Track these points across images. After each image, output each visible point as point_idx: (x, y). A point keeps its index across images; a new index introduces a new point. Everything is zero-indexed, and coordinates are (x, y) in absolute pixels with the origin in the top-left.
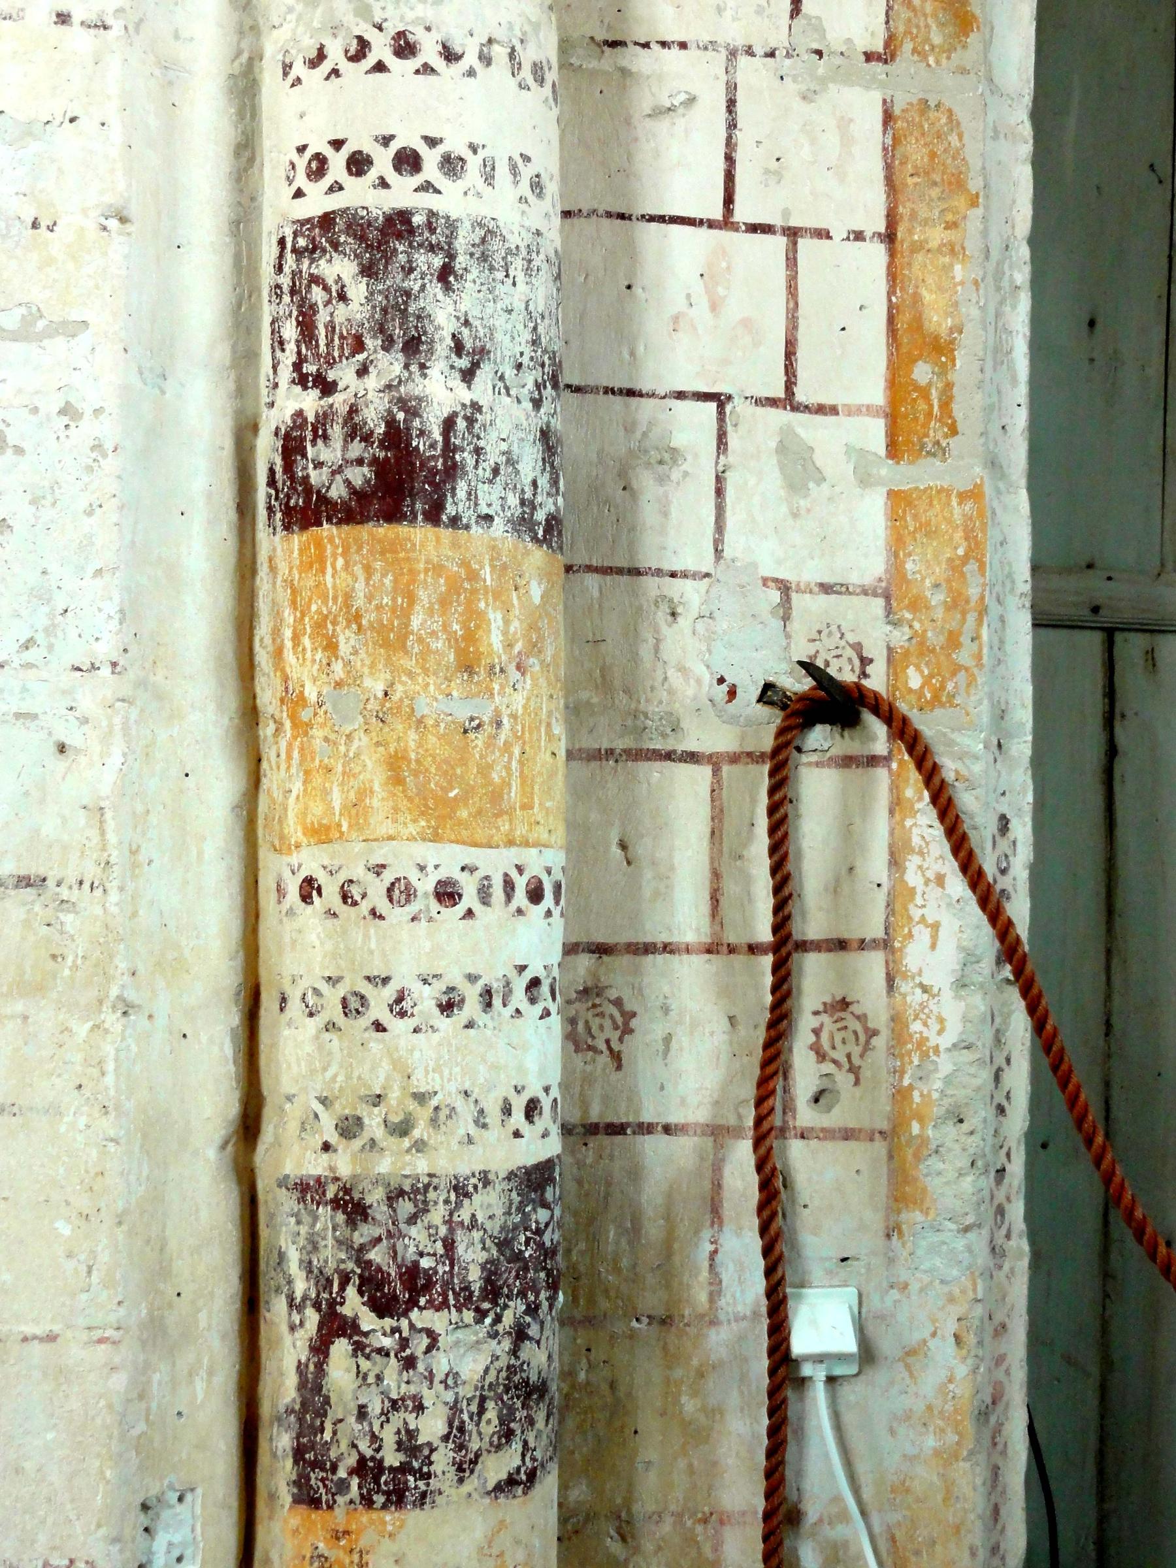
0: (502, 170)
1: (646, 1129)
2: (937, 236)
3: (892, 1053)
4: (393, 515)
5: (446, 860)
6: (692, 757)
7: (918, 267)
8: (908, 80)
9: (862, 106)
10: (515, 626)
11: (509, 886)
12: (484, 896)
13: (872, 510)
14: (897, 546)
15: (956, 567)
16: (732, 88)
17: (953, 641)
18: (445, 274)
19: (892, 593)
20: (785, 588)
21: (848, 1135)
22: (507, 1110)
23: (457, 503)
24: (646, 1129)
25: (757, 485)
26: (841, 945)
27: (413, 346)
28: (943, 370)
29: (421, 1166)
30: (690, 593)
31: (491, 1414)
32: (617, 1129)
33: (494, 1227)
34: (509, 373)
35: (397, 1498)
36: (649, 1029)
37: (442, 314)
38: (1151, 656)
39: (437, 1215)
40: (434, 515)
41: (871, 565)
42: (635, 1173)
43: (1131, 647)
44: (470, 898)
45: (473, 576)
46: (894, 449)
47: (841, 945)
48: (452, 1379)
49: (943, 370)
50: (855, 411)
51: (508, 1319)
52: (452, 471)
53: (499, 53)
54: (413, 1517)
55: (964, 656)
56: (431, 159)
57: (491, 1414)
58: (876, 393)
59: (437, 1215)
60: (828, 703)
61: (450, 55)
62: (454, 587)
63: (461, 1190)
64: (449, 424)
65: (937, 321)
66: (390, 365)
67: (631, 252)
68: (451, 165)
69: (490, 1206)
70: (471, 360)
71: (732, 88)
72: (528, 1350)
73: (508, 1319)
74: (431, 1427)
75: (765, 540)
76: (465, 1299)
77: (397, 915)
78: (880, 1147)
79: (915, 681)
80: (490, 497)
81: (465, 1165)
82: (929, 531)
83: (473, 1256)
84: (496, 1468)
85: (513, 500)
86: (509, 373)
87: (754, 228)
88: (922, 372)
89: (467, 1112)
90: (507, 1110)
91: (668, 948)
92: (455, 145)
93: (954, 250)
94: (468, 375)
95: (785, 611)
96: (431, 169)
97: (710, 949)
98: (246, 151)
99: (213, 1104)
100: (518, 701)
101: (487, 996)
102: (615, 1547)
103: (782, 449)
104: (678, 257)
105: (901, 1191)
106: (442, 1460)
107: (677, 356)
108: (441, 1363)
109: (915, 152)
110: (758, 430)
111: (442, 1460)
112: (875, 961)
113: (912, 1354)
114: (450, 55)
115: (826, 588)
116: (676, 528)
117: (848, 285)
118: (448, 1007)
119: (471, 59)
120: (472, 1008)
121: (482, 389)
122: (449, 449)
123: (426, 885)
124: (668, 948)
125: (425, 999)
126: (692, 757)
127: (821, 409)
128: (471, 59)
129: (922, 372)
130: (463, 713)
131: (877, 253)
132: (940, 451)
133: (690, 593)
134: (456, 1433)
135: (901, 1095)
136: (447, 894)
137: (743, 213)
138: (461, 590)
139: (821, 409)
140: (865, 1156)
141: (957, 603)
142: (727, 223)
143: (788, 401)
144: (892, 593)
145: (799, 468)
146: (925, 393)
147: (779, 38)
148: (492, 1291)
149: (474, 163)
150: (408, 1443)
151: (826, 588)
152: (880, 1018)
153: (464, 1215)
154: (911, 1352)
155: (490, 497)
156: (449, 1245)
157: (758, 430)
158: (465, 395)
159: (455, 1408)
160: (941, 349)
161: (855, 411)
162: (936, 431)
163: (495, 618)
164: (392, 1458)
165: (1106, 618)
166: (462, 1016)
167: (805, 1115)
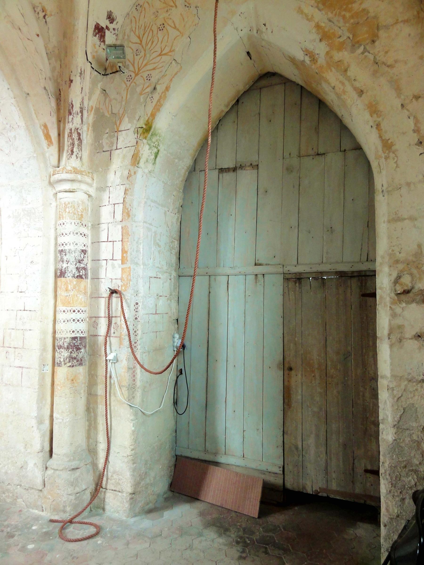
0: (72, 244)
1: (99, 336)
2: (126, 240)
3: (120, 328)
4: (61, 277)
5: (64, 308)
6: (103, 297)
7: (125, 244)
8: (124, 224)
9: (119, 227)
10: (72, 286)
11: (70, 311)
12: (68, 311)
13: (120, 271)
14: (122, 274)
15: (128, 276)
16: (108, 227)
17: (127, 284)
18: (65, 255)
19: (122, 279)
20: (112, 279)
21: (116, 337)
22: (70, 331)
23: (66, 275)
24: (99, 336)
25: (110, 268)
26: (116, 317)
27: (63, 261)
28: (126, 254)
29: (61, 336)
30: (103, 280)
31: (68, 359)
32: (96, 336)
33: (68, 342)
34: (72, 263)
35: (59, 366)
36: (99, 325)
37: (65, 258)
38: (215, 279)
39: (63, 341)
40: (64, 277)
41: (119, 276)
42: (98, 340)
43: (212, 278)
44: (66, 312)
45: (67, 282)
46: (122, 264)
47: (116, 317)
48: (64, 356)
49: (126, 254)
50: (118, 260)
51: (70, 351)
52: (65, 273)
53: (72, 233)
54: (60, 368)
55: (128, 285)
56: (64, 244)
57: (68, 359)
58: (121, 258)
59: (63, 341)
60: (113, 292)
61: (66, 234)
62: (65, 283)
63: (65, 339)
64: (65, 268)
65: (126, 249)
66: (61, 263)
67: (99, 245)
68: (66, 244)
69: (68, 340)
70: (68, 262)
71: (108, 227)
72: (72, 354)
73: (70, 351)
74: (62, 360)
75: (110, 275)
76: (65, 349)
77: (60, 313)
78: (119, 338)
79: (123, 288)
80: (69, 275)
81: (65, 336)
82: (125, 272)
83: (66, 345)
84: (69, 364)
85: (72, 275)
86: (72, 263)
87: (110, 242)
88: (125, 255)
89: (65, 331)
90: (70, 331)
91: (101, 317)
92: (66, 243)
93: (128, 241)
94: (67, 264)
95: (112, 281)
96: (64, 245)
97: (104, 317)
98: (56, 244)
99: (51, 330)
100: (72, 293)
101: (68, 321)
102: (96, 378)
103: (112, 265)
104: (103, 245)
105: (121, 343)
106: (63, 363)
107: (103, 256)
108: (63, 354)
109: (124, 231)
110: (110, 262)
111: (63, 363)
112: (119, 318)
113: (122, 361)
114: (66, 234)
115: (116, 279)
116: (102, 275)
117: (118, 246)
118: (64, 322)
119: (68, 234)
120: (66, 322)
121: (69, 265)
122: (65, 271)
123: (62, 311)
124: (101, 317)
125: (62, 321)
126: (103, 297)
127: (116, 260)
128: (68, 234)
129: (125, 255)
130: (66, 295)
131: (121, 242)
132: (126, 263)
133: (103, 280)
134: (64, 361)
135: (121, 333)
136: (64, 311)
137: (109, 240)
138: (66, 284)
139: (116, 260)
140: (118, 339)
141: (127, 280)
142: (108, 241)
143: (113, 259)
144: (122, 279)
145: (113, 266)
146: (125, 257)
147: (112, 221)
148: (68, 348)
149: (68, 244)
150: (60, 361)
151: (116, 279)
152: (119, 325)
153: (65, 341)
154: (121, 361)
155: (69, 275)
156: (64, 343)
157: (110, 262)
158: (67, 265)
159: (64, 358)
160: (126, 252)
161: (118, 260)
162: (126, 261)
163: (69, 286)
164: (59, 362)
165: (209, 274)
166: (65, 323)
167: (112, 335)
